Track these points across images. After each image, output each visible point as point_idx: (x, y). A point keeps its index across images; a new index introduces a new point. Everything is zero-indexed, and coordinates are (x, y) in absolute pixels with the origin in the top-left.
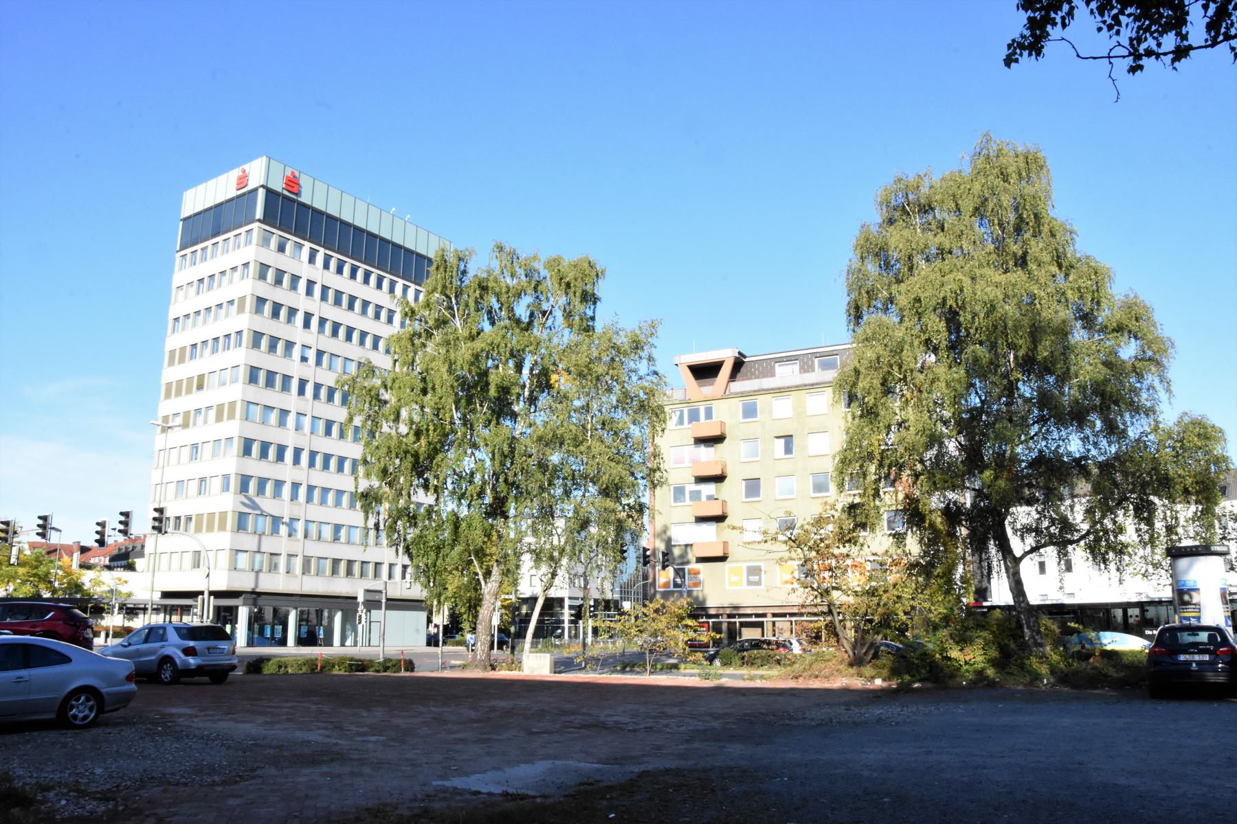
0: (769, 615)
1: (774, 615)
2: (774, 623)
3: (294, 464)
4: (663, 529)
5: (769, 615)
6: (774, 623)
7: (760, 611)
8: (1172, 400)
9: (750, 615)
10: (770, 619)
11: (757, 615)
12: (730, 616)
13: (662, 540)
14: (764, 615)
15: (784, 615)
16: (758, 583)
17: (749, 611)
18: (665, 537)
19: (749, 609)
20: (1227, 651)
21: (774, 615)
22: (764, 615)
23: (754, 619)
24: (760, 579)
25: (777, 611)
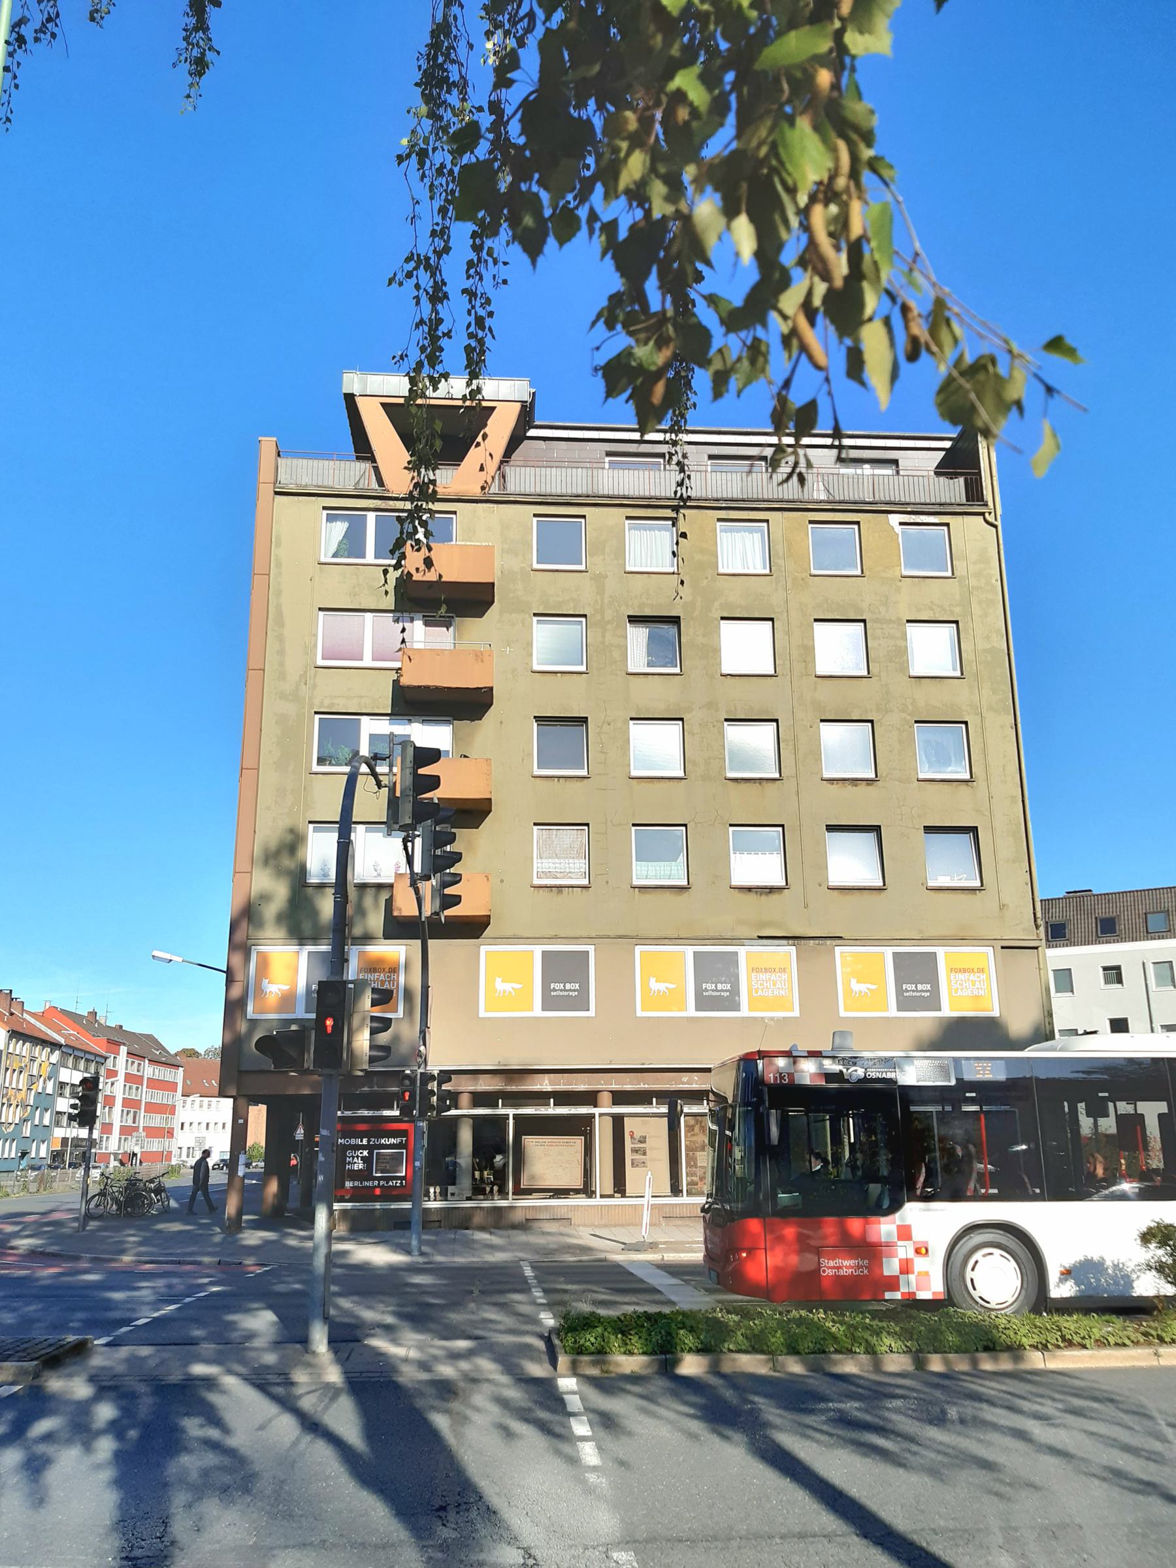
0: (606, 1098)
1: (620, 1098)
2: (618, 1121)
3: (629, 617)
4: (289, 838)
5: (606, 1098)
6: (618, 1121)
7: (581, 1085)
8: (886, 173)
9: (541, 1097)
10: (604, 1110)
11: (563, 1098)
12: (479, 1099)
13: (280, 872)
14: (590, 1098)
15: (642, 1097)
16: (581, 1003)
17: (545, 1084)
18: (287, 863)
19: (685, 1077)
20: (1026, 1174)
21: (620, 1098)
22: (590, 1098)
23: (552, 1110)
24: (735, 991)
25: (628, 1084)
